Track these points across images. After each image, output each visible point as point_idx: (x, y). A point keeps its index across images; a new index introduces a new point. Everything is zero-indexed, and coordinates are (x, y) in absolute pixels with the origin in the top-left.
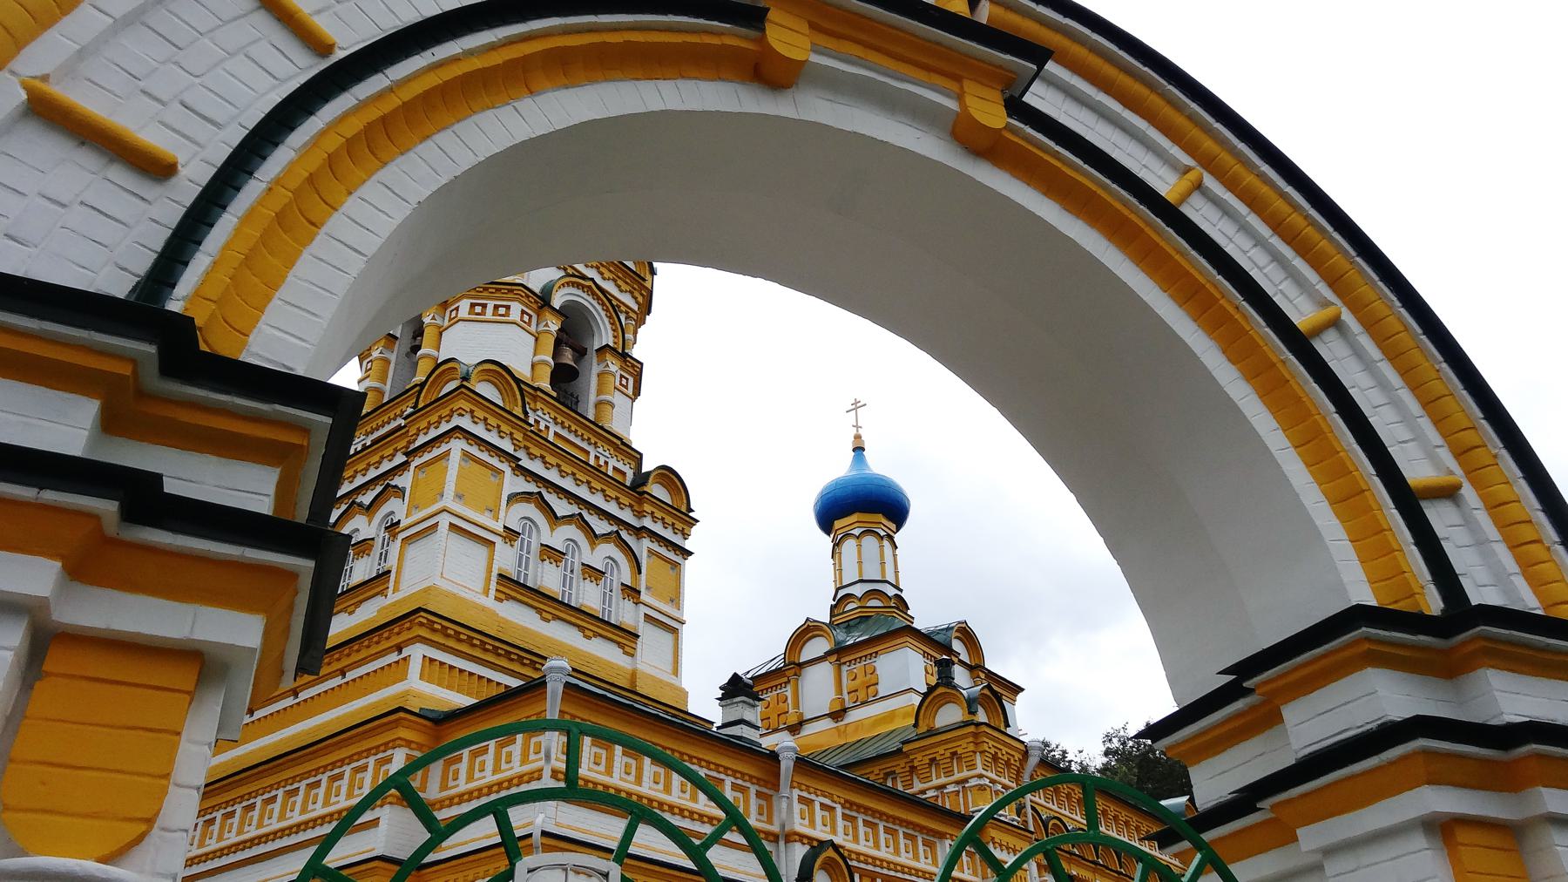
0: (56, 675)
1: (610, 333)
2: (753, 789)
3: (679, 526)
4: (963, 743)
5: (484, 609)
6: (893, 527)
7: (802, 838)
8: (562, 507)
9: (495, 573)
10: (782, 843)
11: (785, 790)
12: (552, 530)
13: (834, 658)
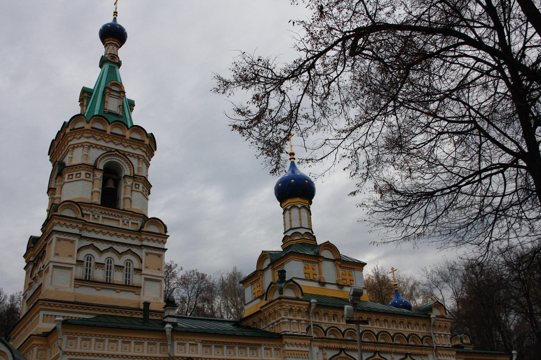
0: (284, 218)
1: (128, 169)
3: (160, 240)
4: (276, 306)
6: (307, 202)
9: (73, 278)
13: (270, 267)
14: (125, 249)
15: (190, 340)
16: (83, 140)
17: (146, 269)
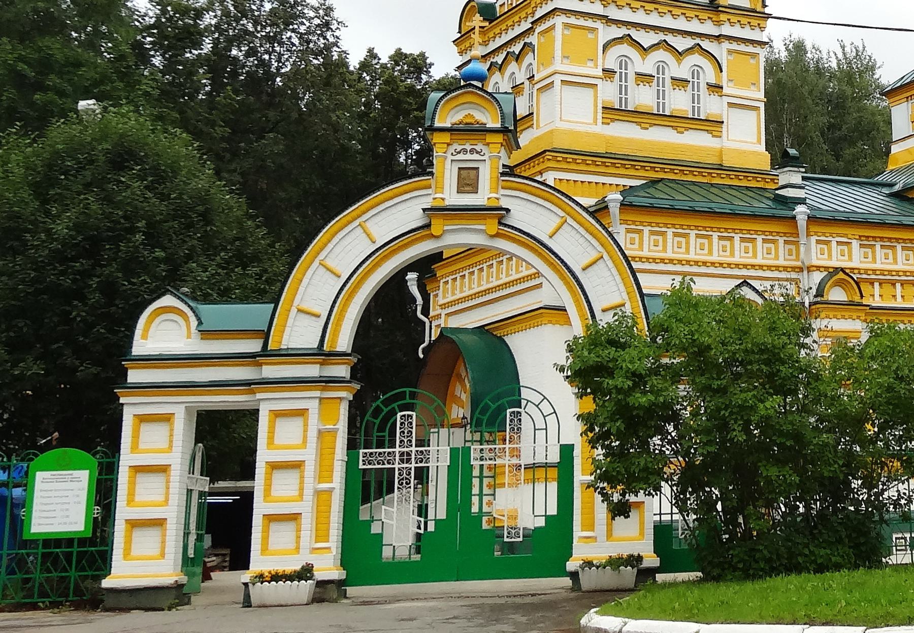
2: (781, 241)
3: (754, 22)
5: (595, 135)
7: (818, 268)
8: (647, 39)
9: (600, 106)
10: (805, 272)
11: (803, 239)
12: (679, 64)
14: (689, 42)
15: (839, 235)
17: (565, 61)
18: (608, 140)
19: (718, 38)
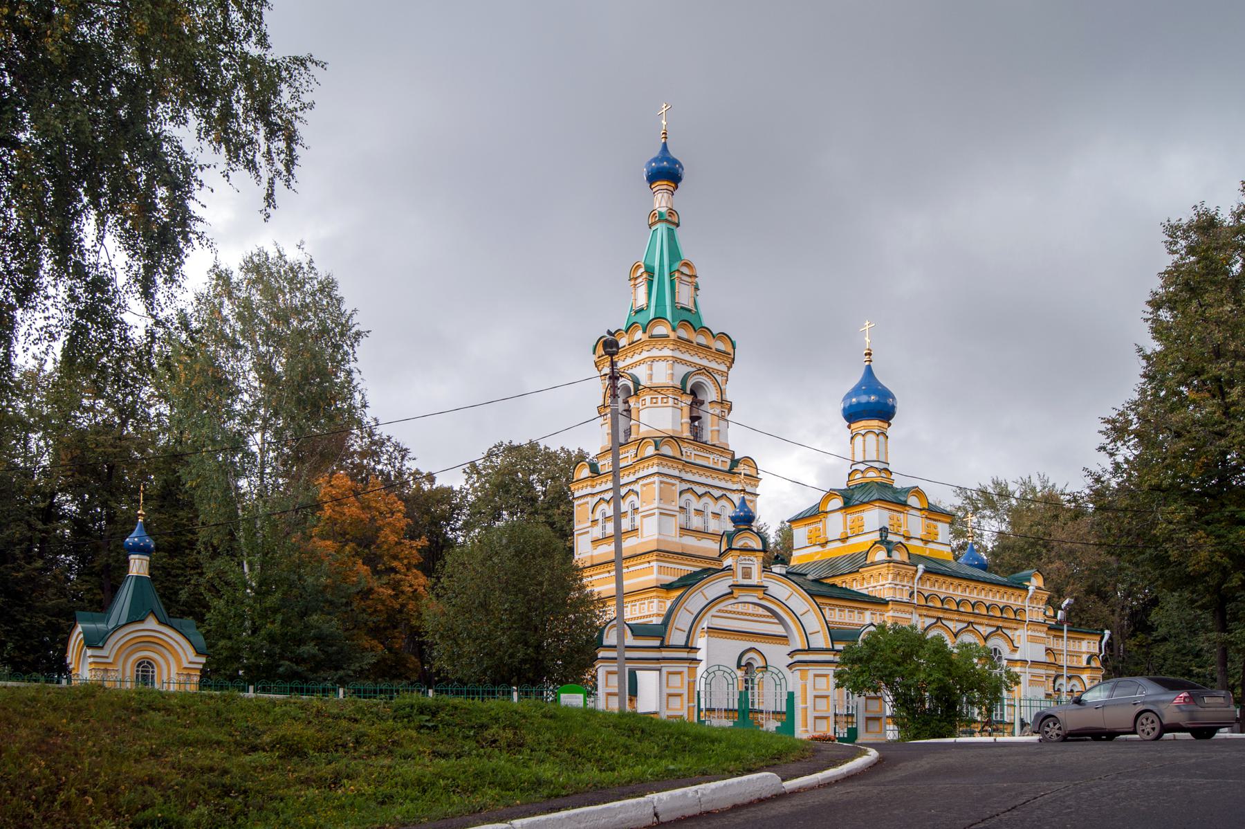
5: (676, 543)
16: (645, 355)
18: (683, 546)
19: (635, 481)
